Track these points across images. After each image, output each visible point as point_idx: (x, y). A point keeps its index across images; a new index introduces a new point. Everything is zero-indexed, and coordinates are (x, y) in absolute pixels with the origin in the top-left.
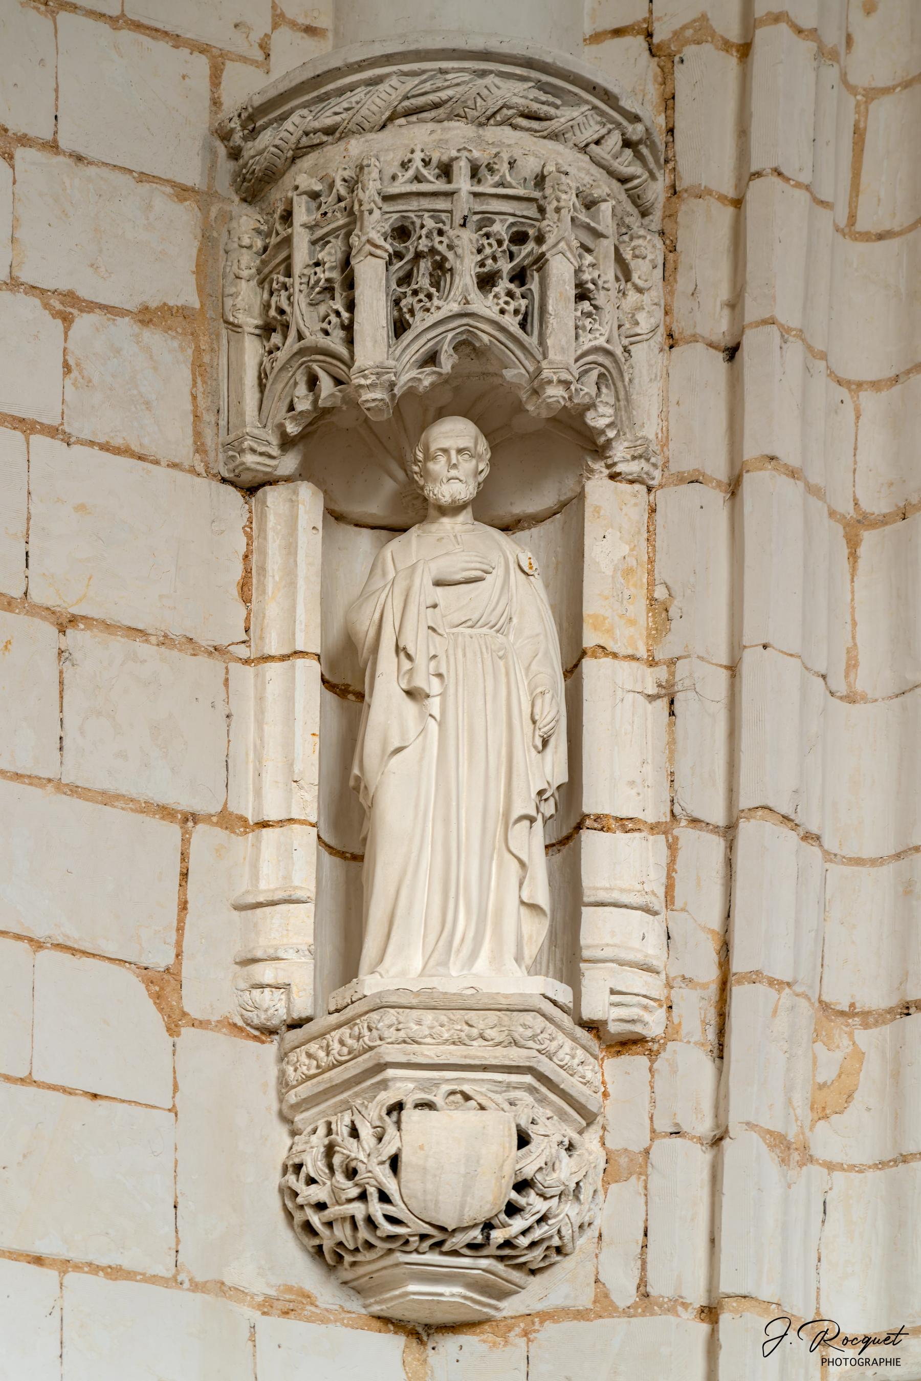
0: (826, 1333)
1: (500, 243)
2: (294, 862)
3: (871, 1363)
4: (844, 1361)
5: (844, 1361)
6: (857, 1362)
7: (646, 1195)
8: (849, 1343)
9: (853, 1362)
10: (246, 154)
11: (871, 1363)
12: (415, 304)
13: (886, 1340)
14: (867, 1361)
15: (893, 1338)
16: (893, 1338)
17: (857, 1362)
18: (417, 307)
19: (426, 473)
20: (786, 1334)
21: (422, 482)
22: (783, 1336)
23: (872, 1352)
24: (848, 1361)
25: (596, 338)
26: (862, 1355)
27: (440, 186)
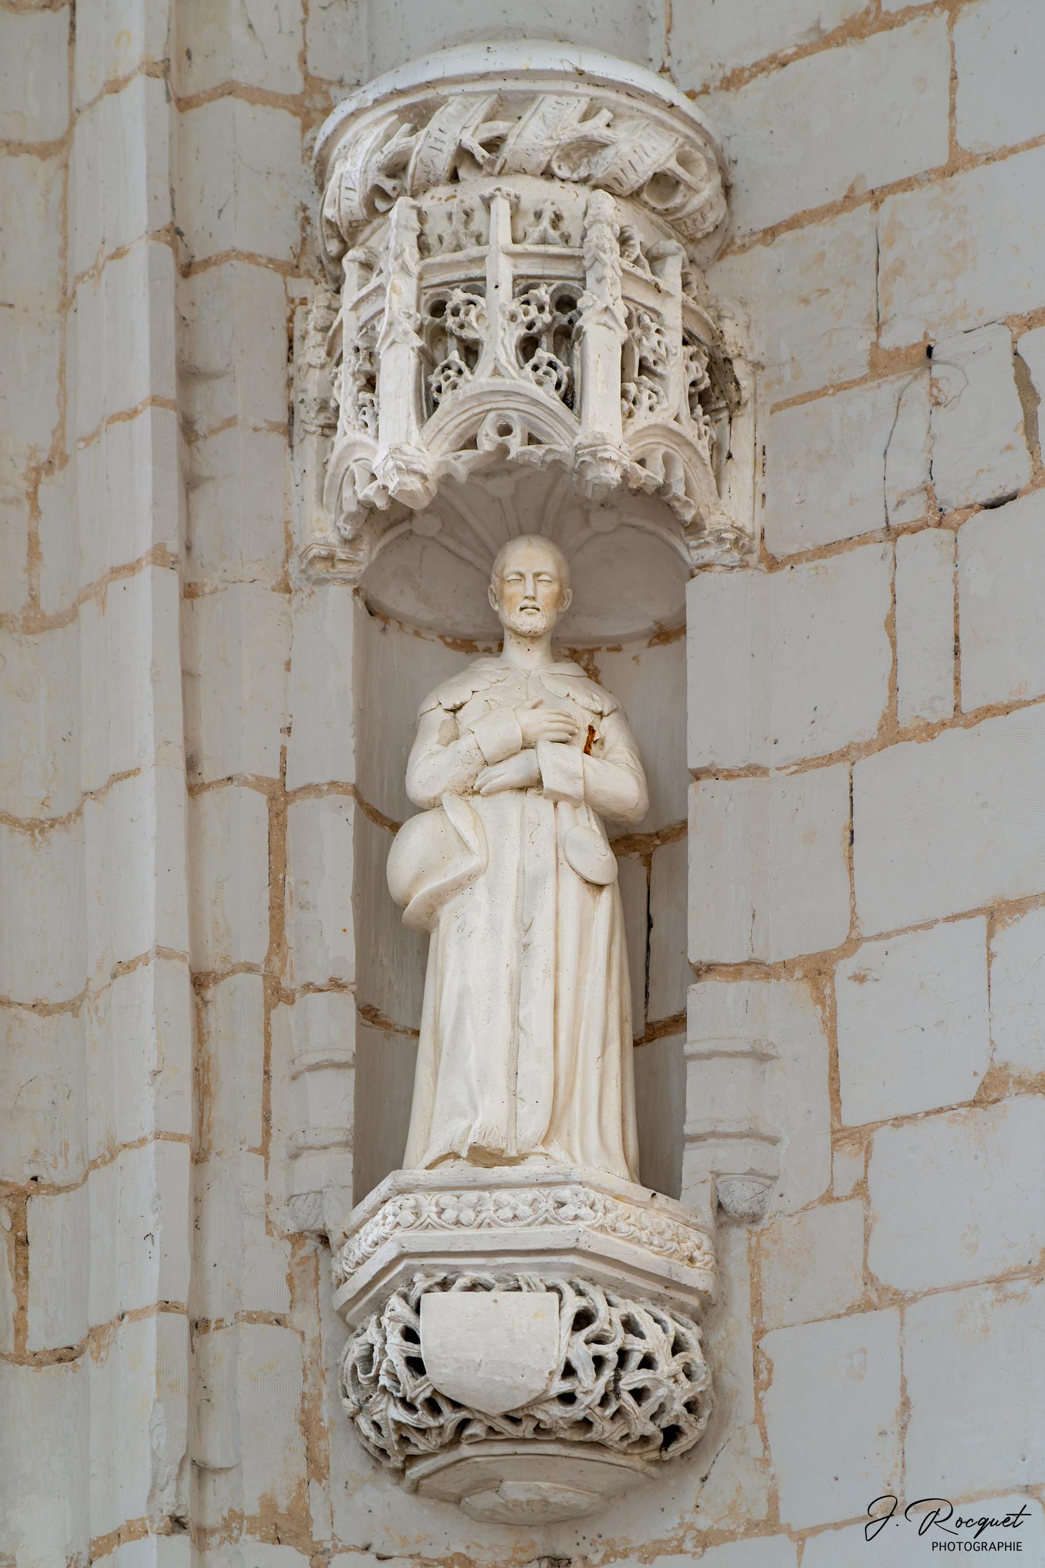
0: (937, 1513)
1: (541, 309)
2: (329, 1025)
3: (988, 1547)
4: (957, 1545)
5: (957, 1545)
6: (973, 1546)
7: (876, 198)
8: (964, 1525)
9: (968, 1546)
10: (365, 345)
11: (988, 1547)
12: (443, 382)
13: (1005, 1521)
14: (984, 1546)
15: (1013, 1519)
16: (1013, 1519)
17: (973, 1546)
18: (444, 385)
19: (500, 597)
20: (891, 1515)
21: (496, 608)
22: (888, 1517)
23: (990, 1535)
24: (962, 1545)
25: (638, 368)
26: (978, 1539)
27: (474, 251)
